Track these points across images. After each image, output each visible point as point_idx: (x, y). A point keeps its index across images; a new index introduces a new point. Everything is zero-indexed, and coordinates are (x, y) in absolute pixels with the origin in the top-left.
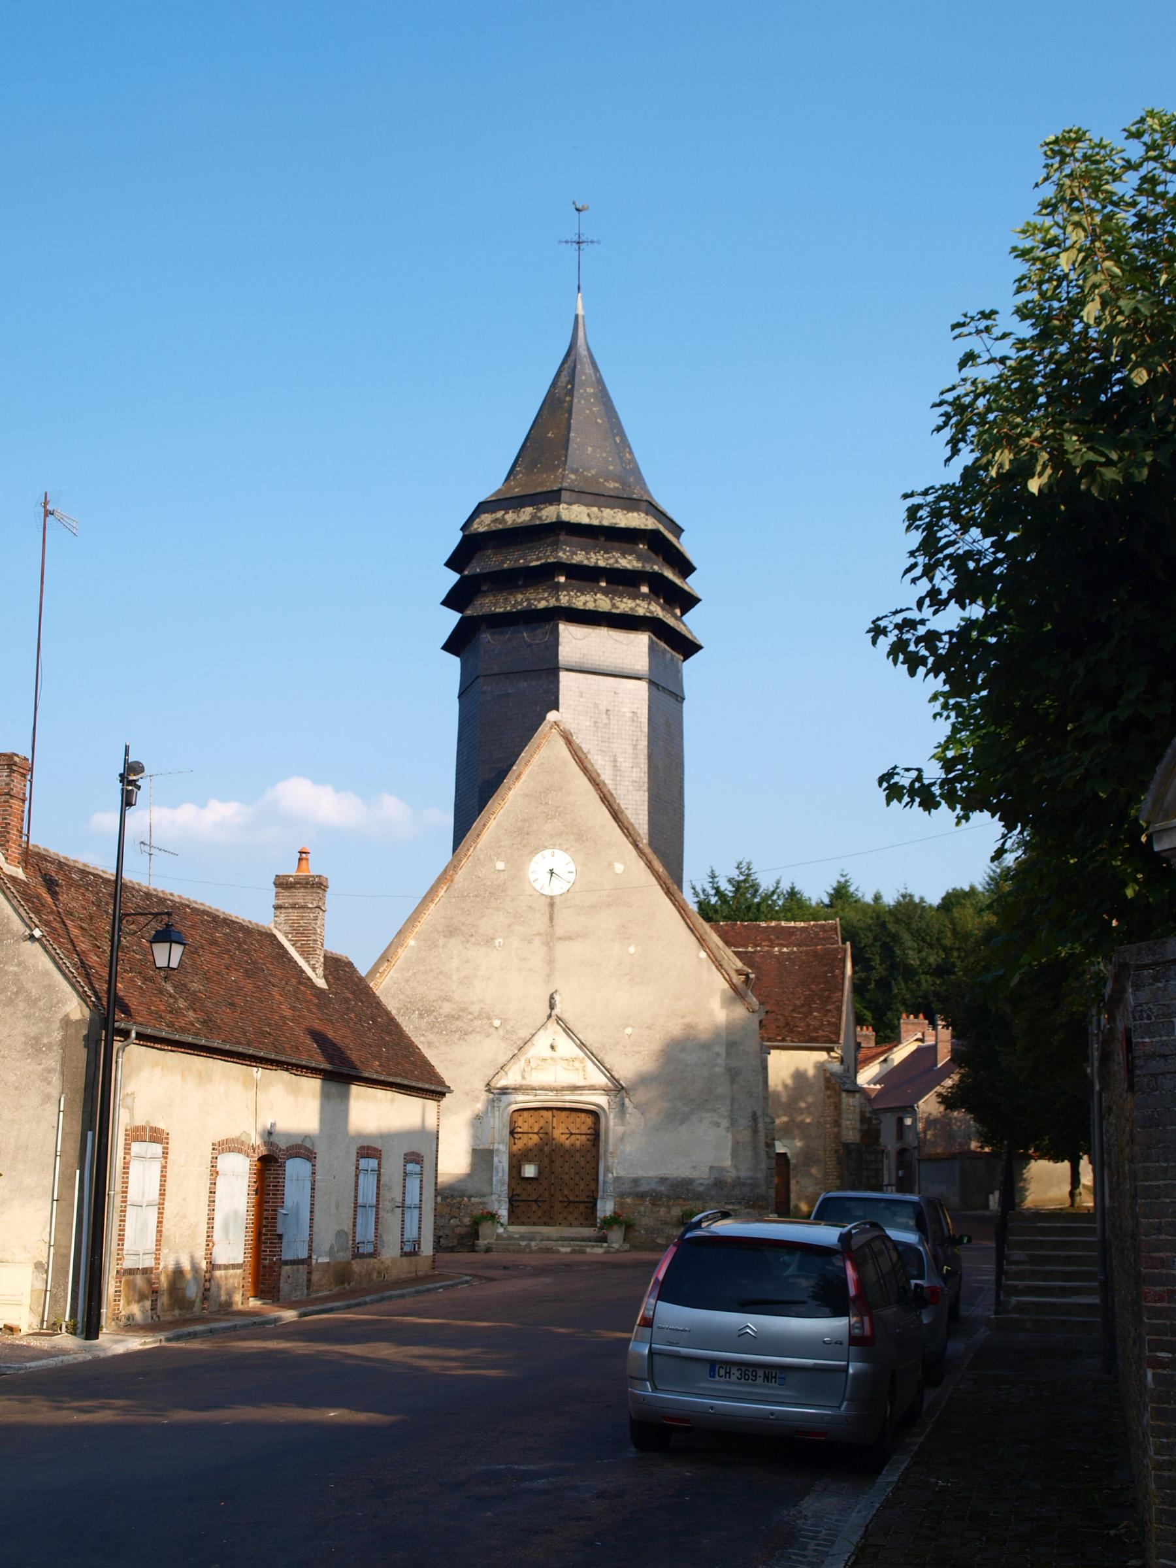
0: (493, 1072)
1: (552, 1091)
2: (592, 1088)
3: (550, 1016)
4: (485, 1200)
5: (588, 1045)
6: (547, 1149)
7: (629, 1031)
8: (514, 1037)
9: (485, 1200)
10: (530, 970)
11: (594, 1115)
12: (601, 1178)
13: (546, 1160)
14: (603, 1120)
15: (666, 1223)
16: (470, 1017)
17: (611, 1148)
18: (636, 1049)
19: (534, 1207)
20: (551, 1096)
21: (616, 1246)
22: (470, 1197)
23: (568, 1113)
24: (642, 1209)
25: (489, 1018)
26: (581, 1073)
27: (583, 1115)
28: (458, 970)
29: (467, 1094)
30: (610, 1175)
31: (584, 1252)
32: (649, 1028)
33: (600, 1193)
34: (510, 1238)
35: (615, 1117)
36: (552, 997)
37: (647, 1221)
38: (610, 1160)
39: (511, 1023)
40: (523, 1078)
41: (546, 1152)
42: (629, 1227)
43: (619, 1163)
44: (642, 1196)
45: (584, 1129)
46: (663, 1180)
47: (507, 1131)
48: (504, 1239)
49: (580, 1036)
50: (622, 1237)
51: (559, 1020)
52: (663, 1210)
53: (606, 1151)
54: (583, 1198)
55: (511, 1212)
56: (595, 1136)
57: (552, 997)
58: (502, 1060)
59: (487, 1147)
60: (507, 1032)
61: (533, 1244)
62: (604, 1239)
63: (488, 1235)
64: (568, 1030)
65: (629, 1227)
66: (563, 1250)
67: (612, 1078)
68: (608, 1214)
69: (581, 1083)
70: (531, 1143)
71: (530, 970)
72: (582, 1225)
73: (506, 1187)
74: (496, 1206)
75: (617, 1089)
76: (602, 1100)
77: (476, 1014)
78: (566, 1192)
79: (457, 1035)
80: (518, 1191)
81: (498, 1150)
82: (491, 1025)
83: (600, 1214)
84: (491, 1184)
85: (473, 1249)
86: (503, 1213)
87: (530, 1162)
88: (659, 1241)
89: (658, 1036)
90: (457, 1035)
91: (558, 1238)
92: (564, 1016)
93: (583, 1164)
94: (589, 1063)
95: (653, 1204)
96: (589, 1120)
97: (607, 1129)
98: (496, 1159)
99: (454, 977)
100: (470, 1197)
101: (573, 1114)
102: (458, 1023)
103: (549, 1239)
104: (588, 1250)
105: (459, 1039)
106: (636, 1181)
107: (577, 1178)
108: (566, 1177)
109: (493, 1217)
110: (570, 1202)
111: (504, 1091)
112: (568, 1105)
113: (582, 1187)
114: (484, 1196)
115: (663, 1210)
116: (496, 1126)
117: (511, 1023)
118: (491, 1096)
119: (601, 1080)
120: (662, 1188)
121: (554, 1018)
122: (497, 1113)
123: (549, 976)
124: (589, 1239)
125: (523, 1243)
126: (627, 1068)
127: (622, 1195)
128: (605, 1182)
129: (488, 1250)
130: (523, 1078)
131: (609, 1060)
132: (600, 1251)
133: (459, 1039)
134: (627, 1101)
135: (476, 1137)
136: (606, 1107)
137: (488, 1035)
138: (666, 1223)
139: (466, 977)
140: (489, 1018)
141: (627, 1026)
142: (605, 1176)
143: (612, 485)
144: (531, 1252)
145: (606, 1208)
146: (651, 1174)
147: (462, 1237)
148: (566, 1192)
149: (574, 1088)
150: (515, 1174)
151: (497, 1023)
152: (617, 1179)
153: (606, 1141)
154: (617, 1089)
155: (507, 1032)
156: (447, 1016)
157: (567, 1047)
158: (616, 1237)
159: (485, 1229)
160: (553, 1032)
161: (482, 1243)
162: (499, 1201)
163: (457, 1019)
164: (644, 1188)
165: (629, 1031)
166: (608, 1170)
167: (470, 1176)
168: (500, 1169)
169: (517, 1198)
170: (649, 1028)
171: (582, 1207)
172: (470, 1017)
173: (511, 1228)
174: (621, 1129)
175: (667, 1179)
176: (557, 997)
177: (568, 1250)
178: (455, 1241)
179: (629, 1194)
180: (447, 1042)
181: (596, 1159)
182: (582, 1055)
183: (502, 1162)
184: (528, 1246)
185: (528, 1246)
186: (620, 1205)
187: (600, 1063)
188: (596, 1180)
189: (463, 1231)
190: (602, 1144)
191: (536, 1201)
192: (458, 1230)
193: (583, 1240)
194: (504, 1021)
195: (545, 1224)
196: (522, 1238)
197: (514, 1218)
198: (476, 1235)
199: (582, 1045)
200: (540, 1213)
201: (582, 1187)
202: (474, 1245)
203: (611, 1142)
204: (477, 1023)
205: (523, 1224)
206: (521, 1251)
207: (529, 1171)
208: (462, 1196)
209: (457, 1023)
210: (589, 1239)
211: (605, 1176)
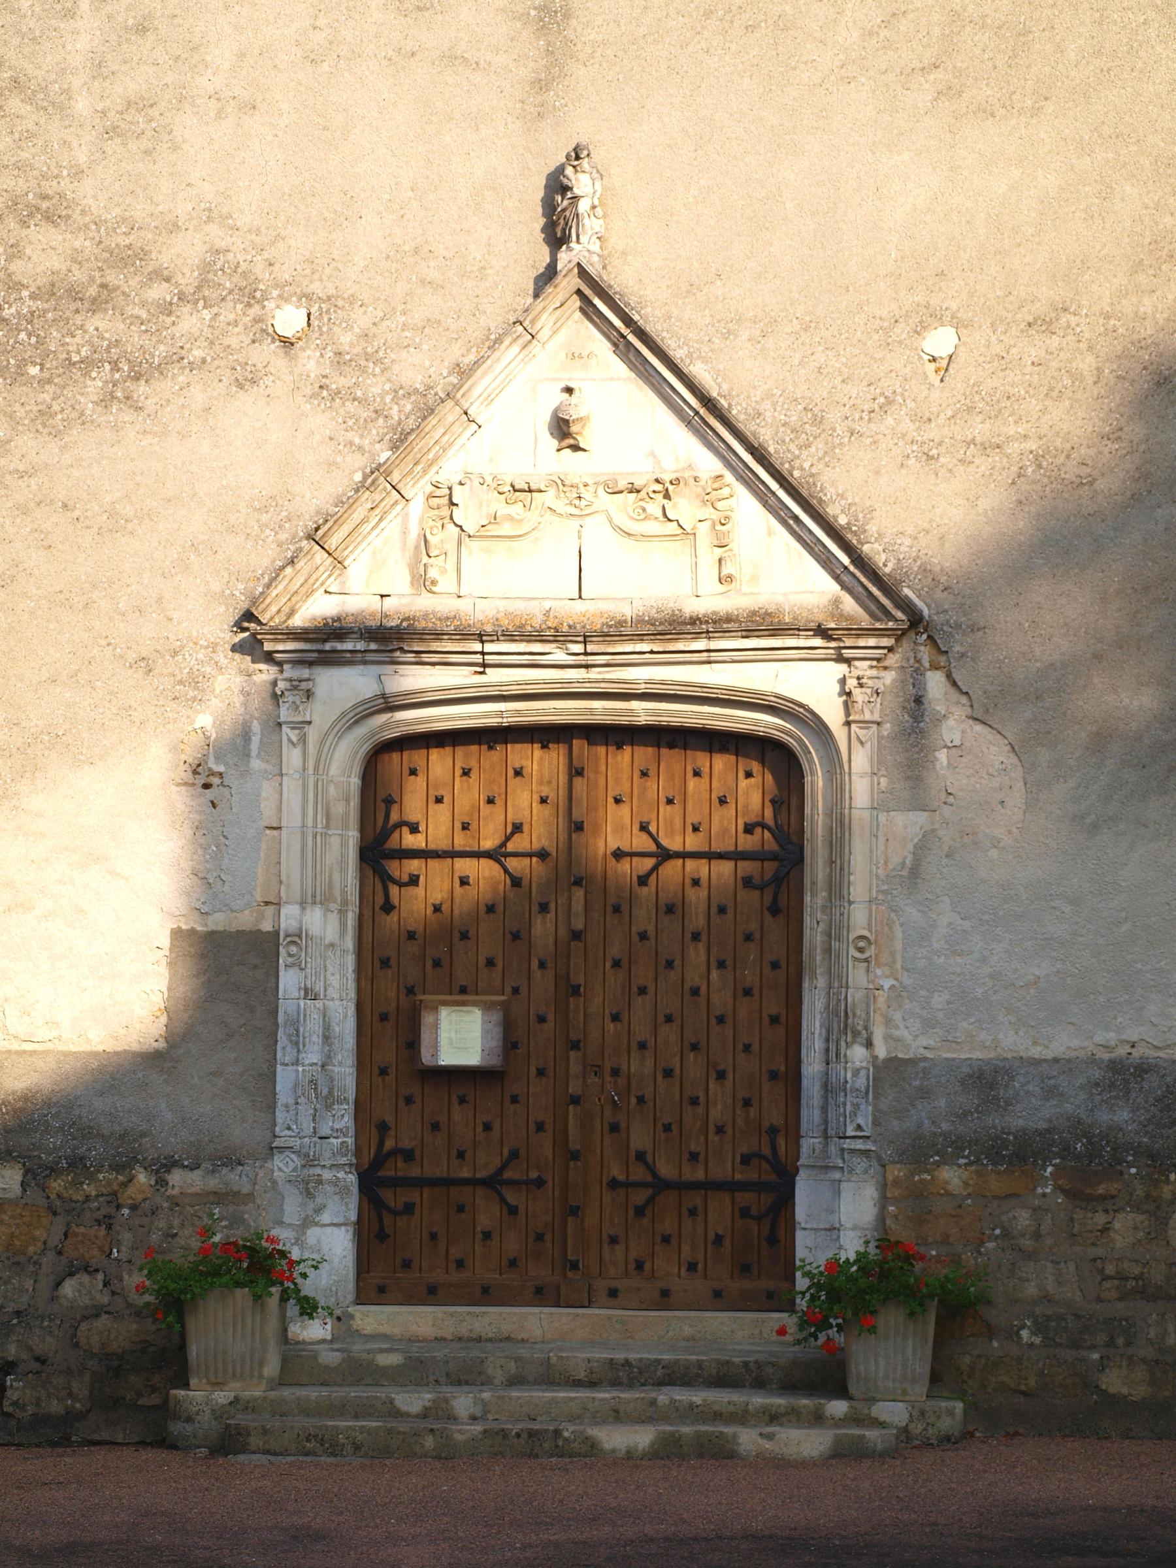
0: (266, 557)
1: (559, 637)
2: (765, 626)
3: (549, 275)
4: (237, 1179)
5: (737, 413)
6: (542, 929)
7: (941, 341)
8: (376, 387)
9: (237, 1179)
10: (451, 58)
11: (776, 756)
12: (812, 1066)
13: (543, 984)
14: (816, 781)
15: (1146, 1292)
16: (159, 292)
17: (859, 919)
18: (980, 429)
19: (487, 1214)
20: (557, 667)
21: (893, 1412)
22: (164, 1166)
23: (643, 754)
24: (1023, 1219)
25: (251, 295)
26: (708, 556)
27: (721, 762)
28: (98, 68)
29: (146, 665)
30: (858, 1054)
31: (719, 1452)
32: (1042, 324)
33: (809, 1144)
34: (358, 1371)
35: (879, 765)
36: (557, 186)
37: (1039, 1281)
38: (857, 976)
39: (361, 319)
40: (422, 581)
41: (557, 934)
42: (958, 1313)
43: (898, 995)
44: (1018, 1154)
45: (725, 828)
46: (1123, 1074)
47: (344, 845)
48: (325, 1377)
49: (699, 371)
50: (922, 1368)
51: (595, 297)
52: (1125, 1227)
53: (835, 931)
54: (725, 1168)
55: (372, 1237)
56: (781, 864)
57: (557, 186)
58: (313, 496)
59: (245, 920)
60: (340, 360)
61: (463, 1402)
62: (828, 1377)
63: (231, 1362)
64: (637, 345)
65: (958, 1313)
66: (617, 1439)
67: (858, 569)
68: (850, 1247)
69: (710, 600)
70: (465, 899)
71: (451, 58)
72: (719, 1300)
73: (343, 1119)
74: (292, 1207)
75: (897, 614)
76: (814, 684)
77: (187, 280)
78: (640, 1137)
79: (95, 386)
80: (406, 1135)
81: (298, 936)
82: (264, 332)
83: (810, 1250)
84: (270, 1105)
85: (159, 1432)
86: (327, 1245)
87: (462, 992)
88: (1114, 1382)
89: (1086, 364)
90: (95, 386)
91: (591, 1366)
92: (622, 278)
93: (721, 999)
94: (744, 504)
95: (1071, 1194)
96: (752, 791)
97: (840, 826)
98: (289, 981)
99: (82, 105)
100: (164, 1166)
101: (672, 759)
102: (102, 324)
103: (551, 1376)
104: (748, 1439)
105: (106, 400)
106: (988, 1081)
107: (695, 1066)
108: (640, 1066)
109: (261, 1268)
110: (661, 1185)
111: (329, 643)
112: (642, 712)
113: (717, 1113)
114: (232, 1160)
115: (1125, 1227)
116: (292, 818)
117: (361, 319)
118: (265, 673)
119: (802, 583)
120: (1120, 1115)
121: (568, 283)
122: (293, 758)
123: (541, 85)
124: (752, 1376)
125: (412, 1401)
126: (931, 510)
127: (919, 1152)
128: (828, 1089)
129: (228, 1442)
130: (422, 581)
131: (843, 487)
132: (808, 1443)
133: (106, 400)
134: (935, 683)
135: (211, 875)
136: (831, 712)
137: (247, 380)
138: (1146, 1292)
139: (139, 104)
140: (251, 295)
141: (932, 317)
142: (832, 1056)
143: (862, 1369)
144: (447, 1454)
145: (839, 1217)
146: (1063, 1043)
147: (115, 1366)
148: (640, 1137)
149: (672, 629)
150: (387, 1054)
151: (289, 319)
152: (891, 1071)
153: (837, 888)
154: (897, 614)
155: (340, 360)
156: (49, 292)
157: (634, 427)
158: (892, 1363)
159: (223, 1329)
160: (572, 354)
161: (201, 1398)
162: (308, 1188)
163: (96, 305)
164: (1029, 1113)
165: (941, 341)
166: (844, 1026)
167: (157, 1062)
168: (312, 1028)
169: (397, 1168)
170: (1042, 324)
171: (720, 1213)
172: (159, 292)
173: (373, 1319)
174: (907, 824)
175: (1143, 1069)
176: (582, 183)
177: (642, 1438)
178: (81, 1387)
179: (952, 1148)
180: (46, 413)
181: (789, 974)
182: (708, 464)
183: (322, 991)
184: (439, 1413)
185: (439, 1413)
186: (908, 1197)
187: (797, 503)
188: (789, 1078)
189: (119, 1333)
190: (814, 902)
191: (493, 1183)
192: (95, 1333)
193: (724, 1379)
194: (321, 311)
195: (542, 1295)
196: (416, 1369)
197: (387, 1264)
198: (172, 1362)
199: (708, 414)
200: (512, 1244)
201: (717, 1113)
202: (166, 1410)
203: (859, 886)
204: (190, 322)
205: (431, 1294)
206: (391, 1448)
207: (460, 1037)
208: (123, 1167)
209: (96, 322)
210: (752, 1376)
211: (832, 1056)
